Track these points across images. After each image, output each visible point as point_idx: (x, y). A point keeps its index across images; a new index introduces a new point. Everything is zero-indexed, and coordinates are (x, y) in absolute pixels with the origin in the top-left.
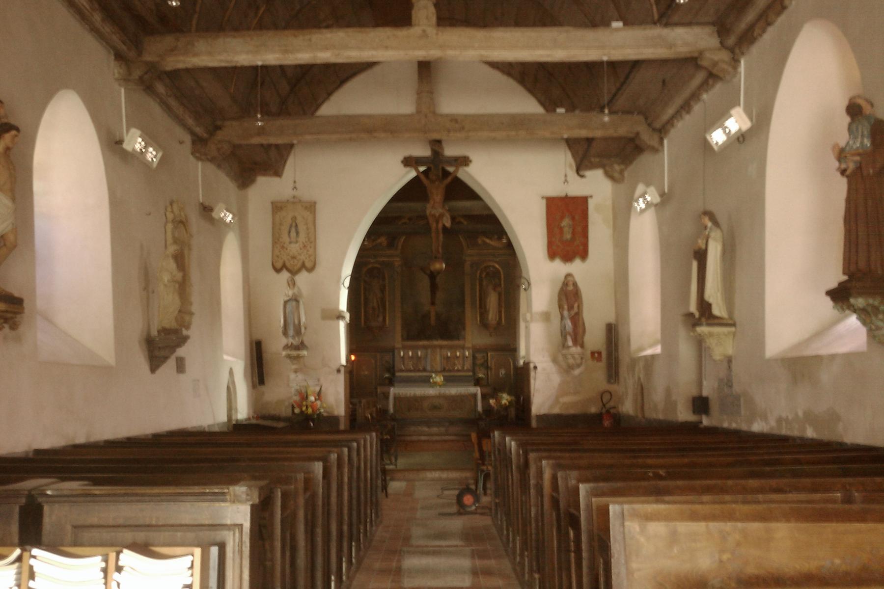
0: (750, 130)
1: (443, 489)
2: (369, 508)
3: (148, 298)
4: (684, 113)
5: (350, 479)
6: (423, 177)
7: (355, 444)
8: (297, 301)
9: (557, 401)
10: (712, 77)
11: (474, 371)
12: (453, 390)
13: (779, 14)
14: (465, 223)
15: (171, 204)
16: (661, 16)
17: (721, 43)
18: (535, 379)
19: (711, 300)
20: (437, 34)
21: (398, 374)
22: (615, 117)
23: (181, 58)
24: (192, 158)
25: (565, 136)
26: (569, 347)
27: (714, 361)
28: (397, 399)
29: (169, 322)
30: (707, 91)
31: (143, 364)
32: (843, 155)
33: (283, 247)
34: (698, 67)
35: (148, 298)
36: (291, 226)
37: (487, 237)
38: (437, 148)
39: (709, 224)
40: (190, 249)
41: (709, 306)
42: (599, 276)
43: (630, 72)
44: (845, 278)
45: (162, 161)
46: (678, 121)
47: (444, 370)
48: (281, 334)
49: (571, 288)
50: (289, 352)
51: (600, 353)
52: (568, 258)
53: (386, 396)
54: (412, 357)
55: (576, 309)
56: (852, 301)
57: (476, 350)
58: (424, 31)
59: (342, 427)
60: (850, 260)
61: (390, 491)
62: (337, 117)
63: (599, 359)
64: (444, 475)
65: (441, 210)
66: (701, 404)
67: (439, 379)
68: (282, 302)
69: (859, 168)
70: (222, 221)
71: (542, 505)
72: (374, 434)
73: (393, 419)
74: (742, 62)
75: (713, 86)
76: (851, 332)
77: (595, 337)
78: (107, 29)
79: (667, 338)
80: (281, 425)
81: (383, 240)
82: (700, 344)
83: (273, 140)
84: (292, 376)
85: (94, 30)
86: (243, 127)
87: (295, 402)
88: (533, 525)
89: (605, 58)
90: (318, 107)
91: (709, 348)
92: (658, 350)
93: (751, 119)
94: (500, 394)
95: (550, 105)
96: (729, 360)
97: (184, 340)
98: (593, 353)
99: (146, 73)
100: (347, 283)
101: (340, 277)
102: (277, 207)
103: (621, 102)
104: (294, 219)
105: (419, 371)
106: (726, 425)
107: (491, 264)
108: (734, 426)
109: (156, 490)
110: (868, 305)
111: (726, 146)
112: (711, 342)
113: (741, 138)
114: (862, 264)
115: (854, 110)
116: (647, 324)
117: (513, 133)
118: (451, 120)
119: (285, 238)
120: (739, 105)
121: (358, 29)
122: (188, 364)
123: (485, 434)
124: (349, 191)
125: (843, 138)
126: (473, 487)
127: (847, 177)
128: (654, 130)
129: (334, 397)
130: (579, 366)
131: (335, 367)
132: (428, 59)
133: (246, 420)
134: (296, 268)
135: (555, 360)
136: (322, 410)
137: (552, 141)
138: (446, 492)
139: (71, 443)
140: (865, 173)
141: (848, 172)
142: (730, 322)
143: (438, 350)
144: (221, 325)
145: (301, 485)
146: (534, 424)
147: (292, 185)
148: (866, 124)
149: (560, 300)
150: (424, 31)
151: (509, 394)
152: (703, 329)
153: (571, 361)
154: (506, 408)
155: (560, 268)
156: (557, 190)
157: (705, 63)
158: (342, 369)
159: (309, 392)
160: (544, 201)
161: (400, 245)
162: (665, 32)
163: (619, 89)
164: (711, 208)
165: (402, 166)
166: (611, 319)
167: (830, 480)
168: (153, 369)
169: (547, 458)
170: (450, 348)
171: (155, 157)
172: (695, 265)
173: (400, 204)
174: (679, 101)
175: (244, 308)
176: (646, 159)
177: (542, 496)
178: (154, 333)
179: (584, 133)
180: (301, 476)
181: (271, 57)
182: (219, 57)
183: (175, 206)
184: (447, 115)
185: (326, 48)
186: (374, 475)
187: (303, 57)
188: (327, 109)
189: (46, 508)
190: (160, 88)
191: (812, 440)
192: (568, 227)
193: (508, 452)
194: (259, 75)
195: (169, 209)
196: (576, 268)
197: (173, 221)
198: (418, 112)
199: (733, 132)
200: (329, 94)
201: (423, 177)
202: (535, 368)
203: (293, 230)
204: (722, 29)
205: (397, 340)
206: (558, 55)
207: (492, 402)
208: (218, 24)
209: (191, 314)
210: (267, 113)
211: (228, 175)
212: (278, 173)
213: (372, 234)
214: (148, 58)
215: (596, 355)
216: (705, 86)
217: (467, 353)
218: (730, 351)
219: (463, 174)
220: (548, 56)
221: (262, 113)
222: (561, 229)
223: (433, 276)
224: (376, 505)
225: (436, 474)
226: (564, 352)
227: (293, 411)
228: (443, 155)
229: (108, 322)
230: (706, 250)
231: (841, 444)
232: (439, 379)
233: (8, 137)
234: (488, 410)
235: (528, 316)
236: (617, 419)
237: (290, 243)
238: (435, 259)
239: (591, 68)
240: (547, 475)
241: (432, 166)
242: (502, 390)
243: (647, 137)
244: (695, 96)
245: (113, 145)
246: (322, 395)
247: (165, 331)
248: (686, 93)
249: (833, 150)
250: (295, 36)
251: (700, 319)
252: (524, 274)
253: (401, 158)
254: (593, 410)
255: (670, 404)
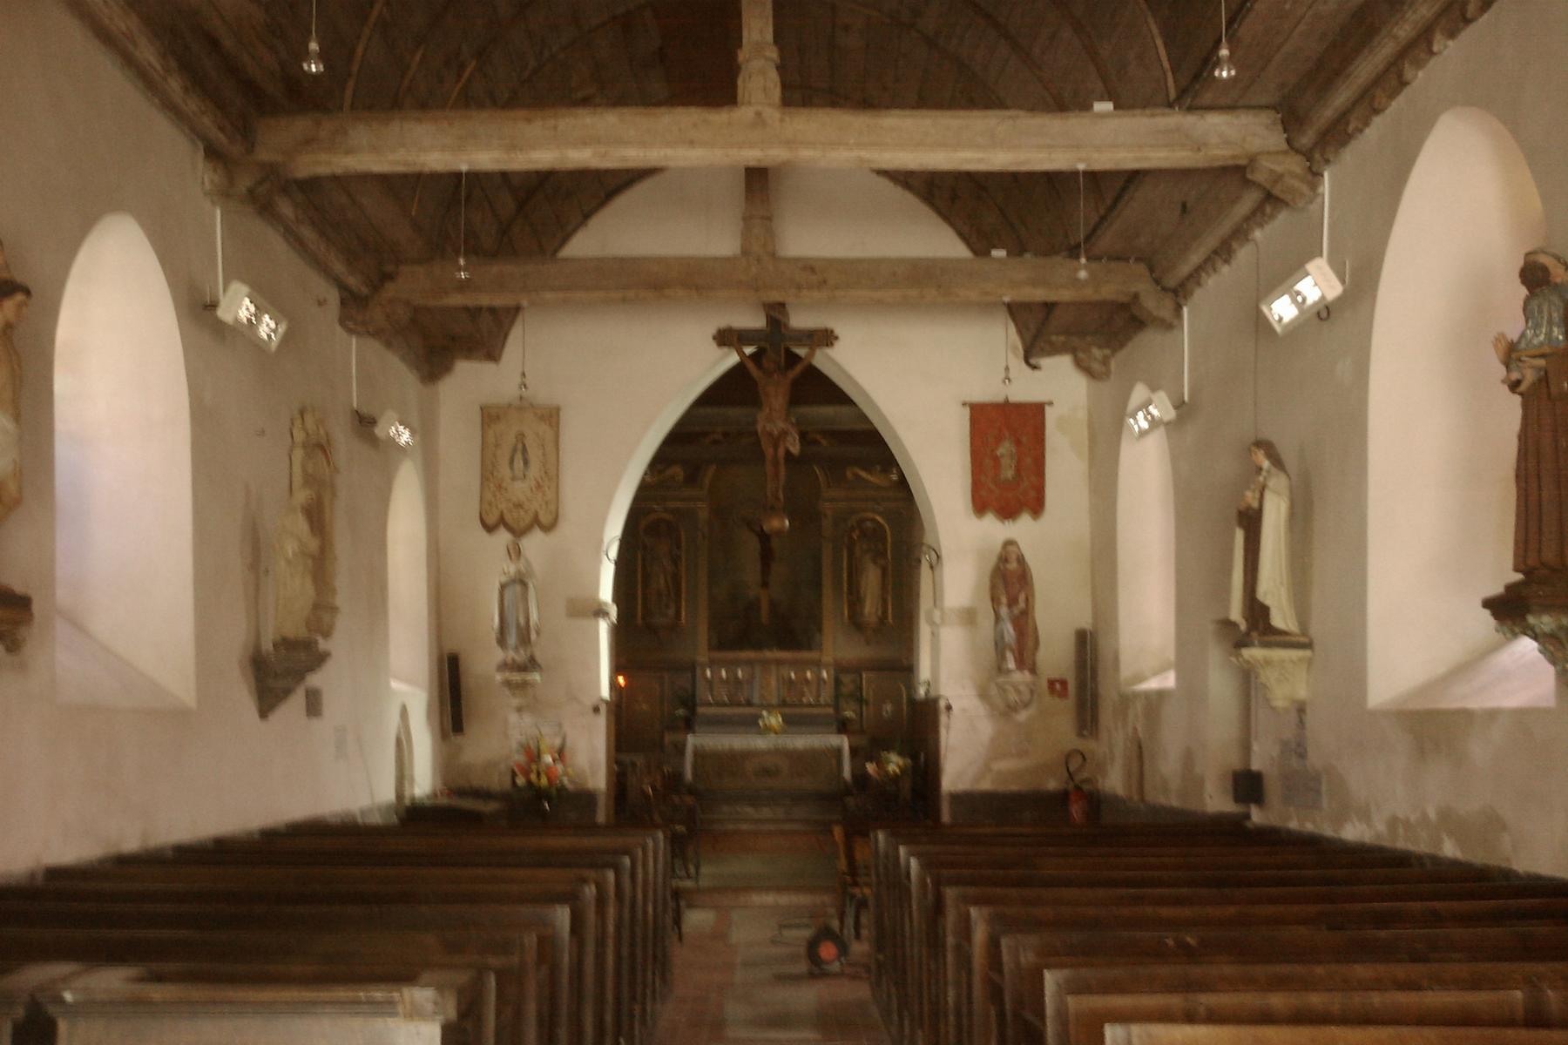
0: (1340, 300)
1: (781, 927)
2: (649, 973)
3: (257, 588)
4: (1219, 263)
5: (618, 928)
6: (751, 366)
7: (627, 861)
8: (524, 584)
9: (987, 768)
10: (1272, 200)
11: (837, 708)
12: (801, 741)
13: (1392, 95)
14: (824, 442)
15: (302, 413)
16: (1182, 93)
17: (1288, 141)
18: (948, 728)
19: (1268, 601)
20: (782, 120)
21: (701, 710)
22: (1094, 265)
23: (324, 157)
24: (339, 329)
25: (1007, 299)
26: (1009, 671)
27: (1273, 708)
28: (699, 755)
29: (294, 628)
30: (1261, 225)
31: (243, 698)
32: (1514, 356)
33: (500, 487)
34: (1248, 183)
35: (257, 588)
36: (515, 450)
37: (865, 469)
38: (776, 315)
39: (1266, 464)
40: (334, 495)
41: (1265, 611)
42: (1068, 553)
43: (1124, 189)
44: (1519, 577)
45: (286, 340)
46: (1209, 275)
47: (783, 704)
48: (494, 643)
49: (1013, 565)
50: (507, 674)
51: (1064, 683)
52: (1008, 512)
53: (680, 749)
54: (727, 682)
55: (1022, 604)
56: (1531, 620)
57: (840, 669)
58: (758, 114)
59: (601, 817)
60: (1526, 542)
61: (686, 929)
62: (601, 260)
63: (1063, 693)
64: (784, 899)
65: (781, 425)
66: (1248, 785)
67: (775, 720)
68: (497, 586)
69: (1544, 379)
70: (392, 443)
71: (970, 987)
72: (660, 835)
73: (692, 791)
74: (1326, 175)
75: (1272, 217)
76: (1523, 671)
77: (1055, 653)
78: (192, 105)
79: (1187, 660)
80: (491, 807)
81: (677, 471)
82: (1247, 679)
83: (485, 300)
84: (513, 718)
85: (170, 108)
86: (435, 278)
87: (519, 766)
88: (951, 1018)
89: (1081, 167)
90: (565, 239)
91: (1265, 686)
92: (1169, 681)
93: (1343, 282)
94: (884, 754)
95: (980, 242)
96: (1301, 709)
97: (320, 659)
98: (1051, 683)
99: (260, 183)
100: (613, 552)
101: (601, 541)
102: (490, 416)
103: (1106, 241)
104: (521, 436)
105: (739, 705)
106: (1293, 825)
107: (870, 515)
108: (1309, 827)
109: (267, 994)
110: (1561, 628)
111: (1296, 328)
112: (1269, 676)
113: (1324, 313)
114: (1549, 555)
115: (1534, 276)
116: (1150, 635)
117: (914, 293)
118: (805, 268)
119: (504, 471)
120: (1321, 255)
121: (641, 110)
122: (329, 704)
123: (858, 829)
124: (618, 390)
125: (1513, 326)
126: (835, 924)
127: (1521, 394)
128: (1164, 289)
129: (588, 756)
130: (1026, 705)
131: (589, 702)
132: (763, 164)
133: (428, 797)
134: (522, 524)
135: (983, 695)
136: (566, 781)
137: (985, 307)
138: (787, 933)
139: (112, 850)
140: (1554, 390)
141: (1523, 388)
142: (1303, 640)
143: (773, 668)
144: (386, 636)
145: (531, 956)
146: (946, 817)
147: (518, 379)
148: (1555, 299)
149: (993, 587)
150: (758, 114)
151: (900, 754)
152: (1254, 653)
153: (1013, 697)
154: (895, 779)
155: (994, 530)
156: (989, 390)
157: (1259, 177)
158: (603, 709)
159: (543, 747)
160: (967, 411)
161: (707, 481)
162: (1190, 121)
163: (1103, 218)
164: (1268, 434)
165: (714, 345)
166: (1085, 622)
167: (1505, 967)
168: (264, 713)
169: (978, 901)
170: (794, 664)
171: (275, 331)
172: (1239, 536)
173: (709, 411)
174: (1211, 241)
175: (429, 594)
176: (1149, 340)
177: (970, 972)
178: (267, 646)
179: (1039, 294)
180: (531, 940)
181: (484, 157)
182: (391, 157)
183: (309, 419)
184: (797, 260)
185: (585, 143)
186: (660, 908)
187: (543, 157)
188: (585, 244)
189: (63, 1026)
190: (286, 208)
191: (1455, 863)
192: (1009, 458)
193: (903, 870)
194: (460, 189)
195: (298, 423)
196: (1023, 530)
197: (305, 446)
198: (745, 252)
199: (1309, 301)
200: (587, 216)
201: (751, 366)
202: (949, 708)
203: (519, 456)
204: (1291, 117)
205: (702, 656)
206: (999, 160)
207: (871, 768)
208: (390, 97)
209: (334, 610)
210: (475, 250)
211: (403, 359)
212: (493, 355)
213: (660, 461)
214: (264, 155)
215: (1058, 686)
216: (1258, 215)
217: (825, 674)
218: (1302, 693)
219: (823, 360)
220: (980, 160)
221: (466, 256)
222: (996, 460)
223: (764, 538)
224: (662, 963)
225: (769, 899)
226: (1001, 680)
227: (514, 783)
228: (786, 326)
229: (185, 627)
230: (1260, 511)
231: (1508, 874)
232: (775, 720)
233: (10, 305)
234: (861, 779)
235: (937, 614)
236: (1095, 801)
237: (514, 479)
238: (773, 509)
239: (1052, 179)
240: (980, 934)
241: (763, 344)
242: (888, 748)
243: (1152, 302)
244: (1240, 233)
245: (198, 309)
246: (567, 753)
247: (287, 644)
248: (1225, 227)
249: (1496, 346)
250: (529, 121)
251: (1248, 634)
252: (928, 539)
253: (713, 331)
254: (1052, 785)
255: (1192, 781)
